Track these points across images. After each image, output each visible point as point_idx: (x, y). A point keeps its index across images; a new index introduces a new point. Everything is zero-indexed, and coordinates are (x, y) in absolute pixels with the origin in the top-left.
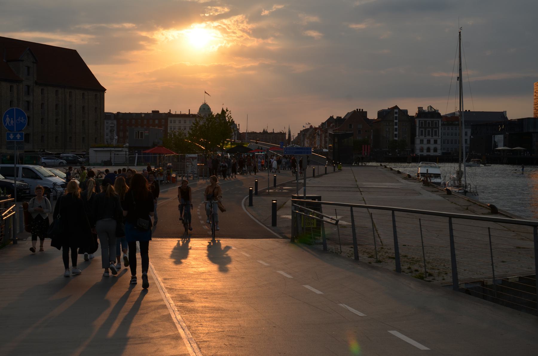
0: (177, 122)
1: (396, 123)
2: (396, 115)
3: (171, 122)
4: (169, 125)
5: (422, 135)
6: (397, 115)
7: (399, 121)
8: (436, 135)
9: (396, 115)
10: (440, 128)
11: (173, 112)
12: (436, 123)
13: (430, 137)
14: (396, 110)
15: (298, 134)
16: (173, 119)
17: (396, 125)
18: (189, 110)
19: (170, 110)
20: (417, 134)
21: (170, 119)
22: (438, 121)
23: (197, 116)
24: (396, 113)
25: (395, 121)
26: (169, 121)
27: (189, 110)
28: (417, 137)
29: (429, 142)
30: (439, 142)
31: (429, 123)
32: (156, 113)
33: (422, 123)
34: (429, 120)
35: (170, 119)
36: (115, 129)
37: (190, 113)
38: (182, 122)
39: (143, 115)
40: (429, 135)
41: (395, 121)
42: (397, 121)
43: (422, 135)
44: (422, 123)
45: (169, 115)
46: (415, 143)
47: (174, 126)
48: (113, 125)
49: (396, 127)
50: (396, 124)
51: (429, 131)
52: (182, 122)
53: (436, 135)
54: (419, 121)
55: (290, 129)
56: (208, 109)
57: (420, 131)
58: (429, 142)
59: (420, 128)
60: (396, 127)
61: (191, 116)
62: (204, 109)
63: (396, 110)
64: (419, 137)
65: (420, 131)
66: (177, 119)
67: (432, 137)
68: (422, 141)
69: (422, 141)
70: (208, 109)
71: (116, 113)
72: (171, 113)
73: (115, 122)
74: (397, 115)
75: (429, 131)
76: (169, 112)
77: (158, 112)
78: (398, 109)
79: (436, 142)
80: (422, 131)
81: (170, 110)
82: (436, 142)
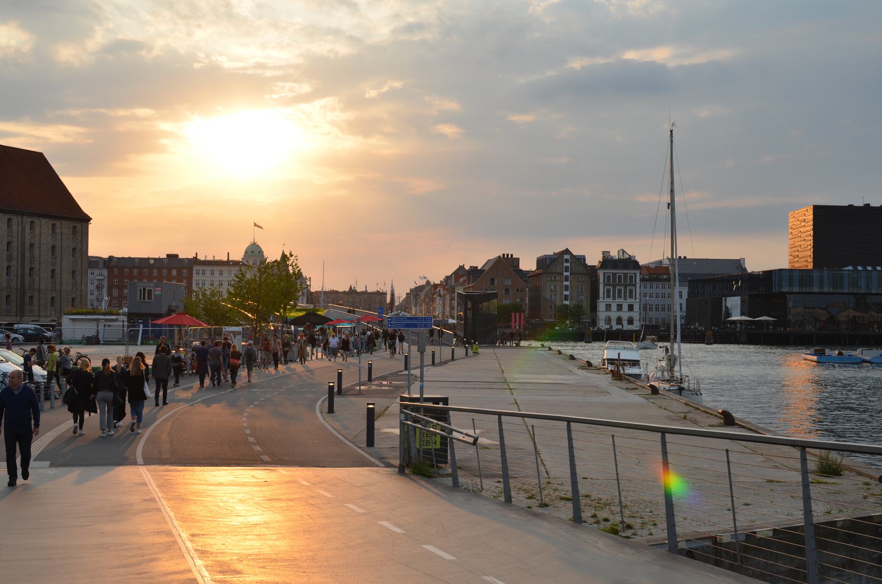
0: (208, 273)
1: (567, 277)
2: (566, 264)
3: (198, 273)
4: (194, 278)
5: (608, 296)
6: (568, 265)
7: (571, 274)
8: (631, 296)
9: (566, 264)
10: (638, 286)
11: (201, 257)
12: (631, 278)
13: (611, 300)
14: (567, 257)
15: (407, 294)
16: (201, 268)
17: (567, 280)
18: (228, 253)
19: (197, 253)
20: (601, 295)
21: (195, 268)
22: (635, 274)
23: (241, 263)
24: (567, 261)
25: (566, 274)
26: (194, 272)
27: (228, 253)
28: (601, 300)
29: (620, 307)
30: (636, 307)
31: (620, 277)
32: (172, 257)
33: (609, 277)
34: (620, 272)
35: (195, 268)
36: (105, 283)
37: (230, 259)
38: (217, 273)
39: (152, 262)
40: (620, 296)
41: (566, 274)
42: (568, 274)
43: (608, 296)
44: (609, 277)
45: (195, 261)
46: (598, 310)
47: (202, 280)
48: (102, 278)
49: (567, 283)
50: (567, 279)
51: (620, 291)
52: (217, 273)
53: (631, 296)
54: (604, 274)
55: (394, 286)
56: (260, 252)
57: (606, 291)
58: (620, 307)
59: (605, 285)
60: (567, 283)
61: (231, 263)
62: (253, 252)
63: (567, 257)
64: (604, 299)
65: (606, 291)
66: (208, 269)
67: (624, 300)
68: (608, 307)
69: (608, 307)
70: (260, 252)
71: (108, 257)
72: (198, 258)
73: (105, 272)
74: (568, 265)
75: (620, 291)
76: (195, 256)
77: (177, 256)
78: (571, 254)
79: (631, 308)
80: (608, 291)
81: (197, 253)
82: (631, 308)
